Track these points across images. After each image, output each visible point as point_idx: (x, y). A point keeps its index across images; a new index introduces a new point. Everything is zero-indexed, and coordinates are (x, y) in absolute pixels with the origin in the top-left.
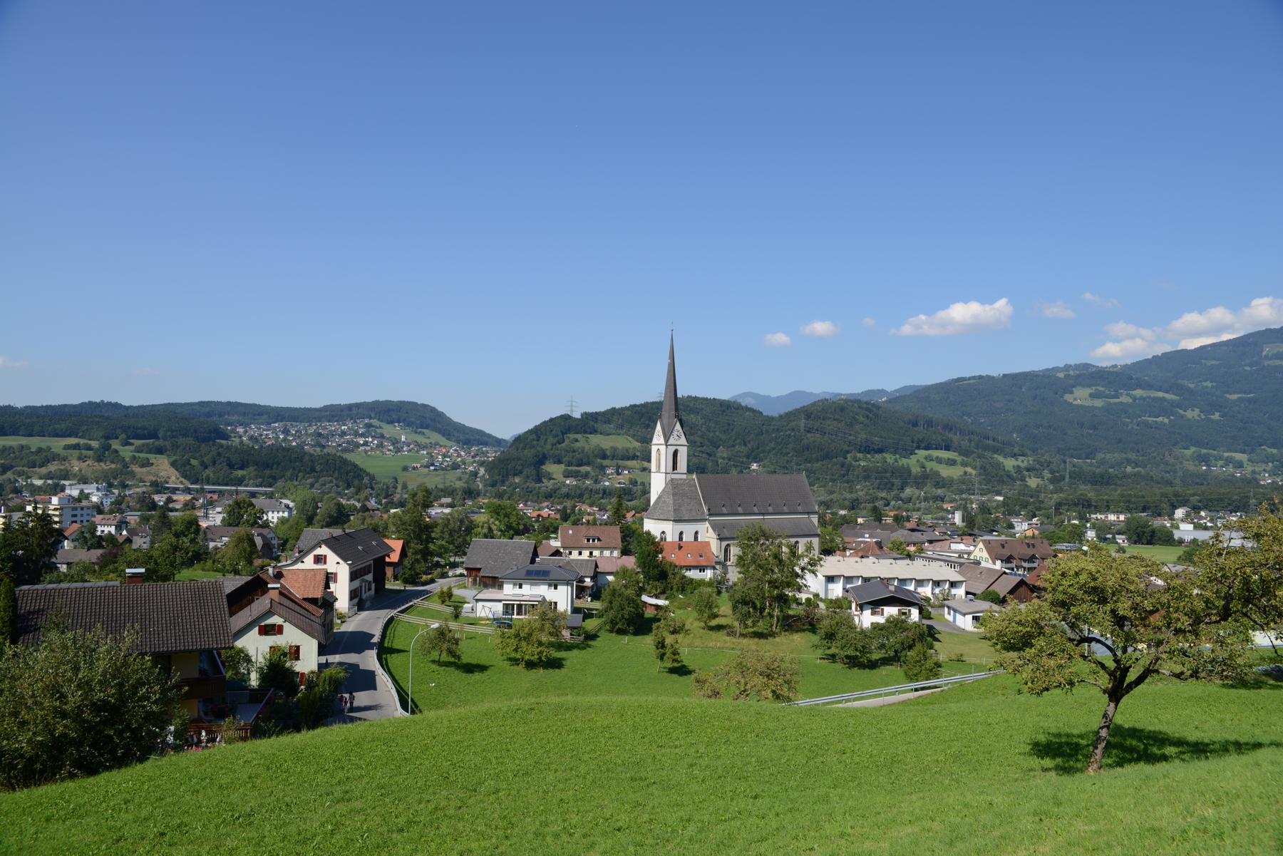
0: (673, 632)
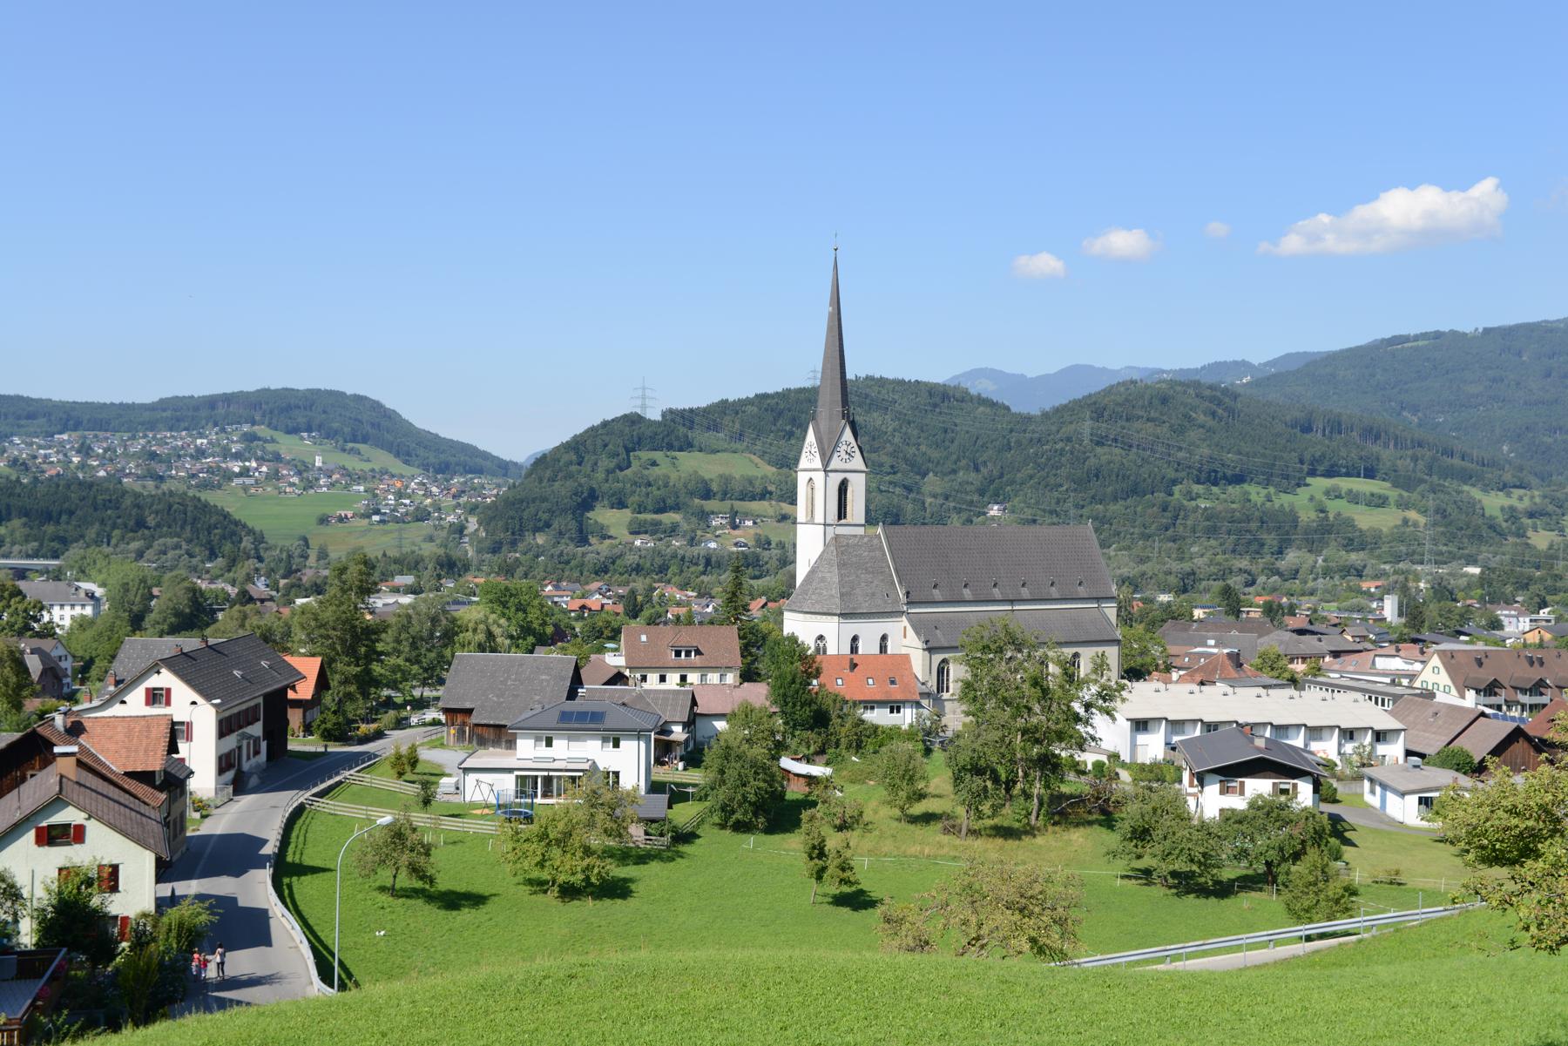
0: (841, 828)
